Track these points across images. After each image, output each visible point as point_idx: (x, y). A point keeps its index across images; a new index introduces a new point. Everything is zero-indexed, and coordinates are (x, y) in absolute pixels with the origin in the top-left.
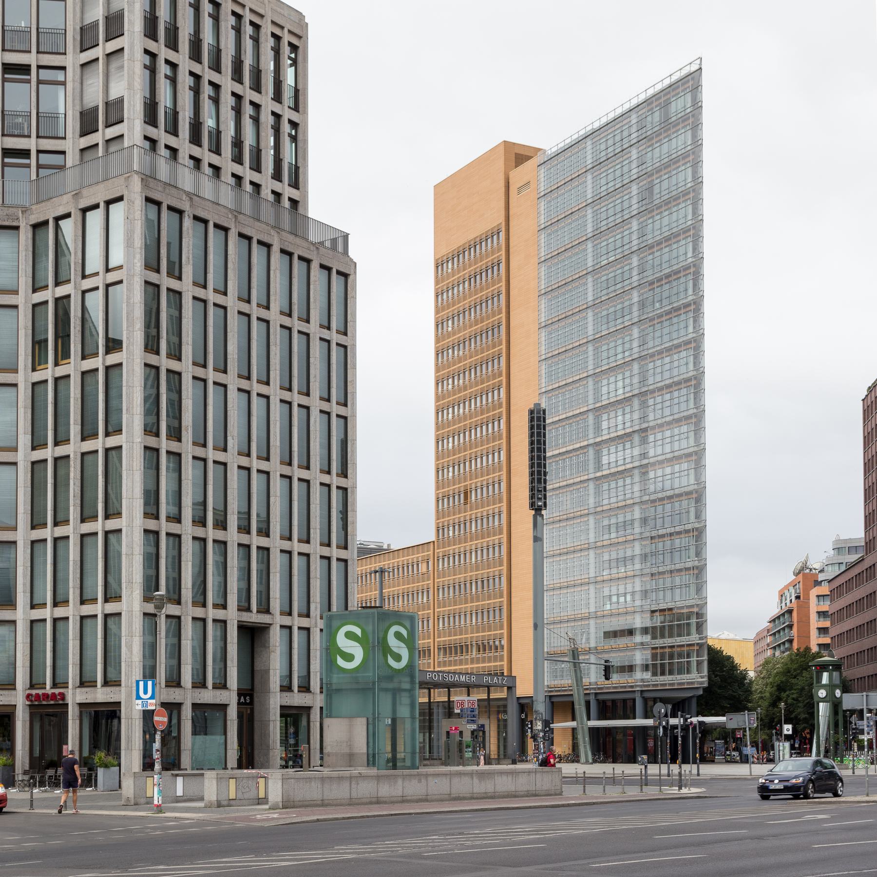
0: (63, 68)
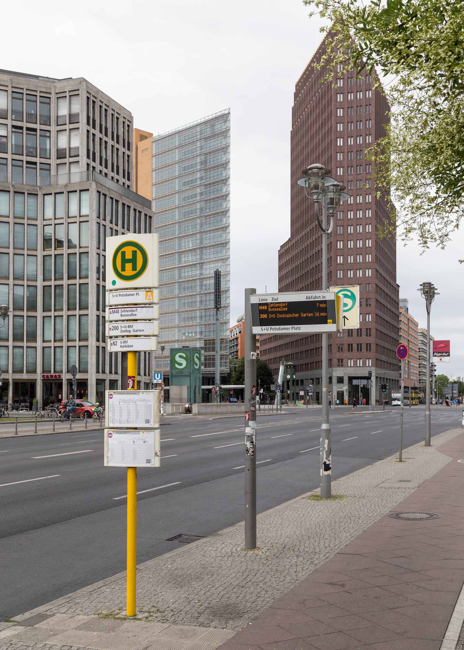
0: (50, 131)
